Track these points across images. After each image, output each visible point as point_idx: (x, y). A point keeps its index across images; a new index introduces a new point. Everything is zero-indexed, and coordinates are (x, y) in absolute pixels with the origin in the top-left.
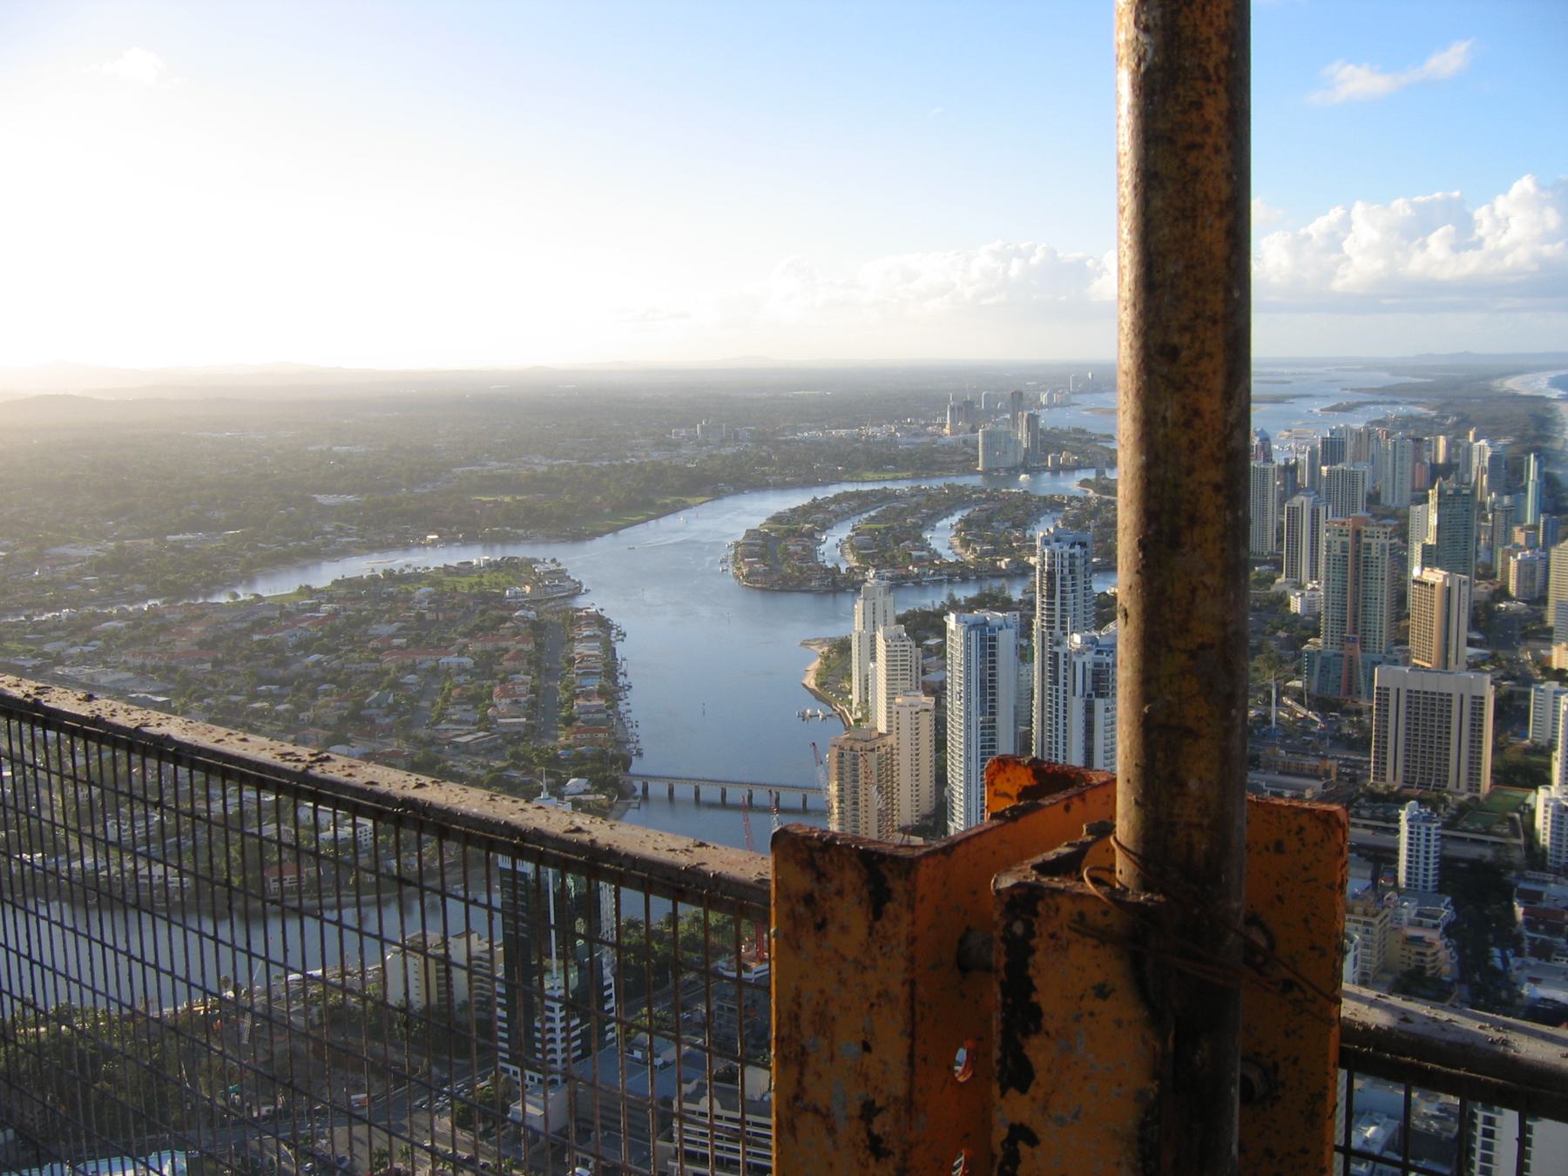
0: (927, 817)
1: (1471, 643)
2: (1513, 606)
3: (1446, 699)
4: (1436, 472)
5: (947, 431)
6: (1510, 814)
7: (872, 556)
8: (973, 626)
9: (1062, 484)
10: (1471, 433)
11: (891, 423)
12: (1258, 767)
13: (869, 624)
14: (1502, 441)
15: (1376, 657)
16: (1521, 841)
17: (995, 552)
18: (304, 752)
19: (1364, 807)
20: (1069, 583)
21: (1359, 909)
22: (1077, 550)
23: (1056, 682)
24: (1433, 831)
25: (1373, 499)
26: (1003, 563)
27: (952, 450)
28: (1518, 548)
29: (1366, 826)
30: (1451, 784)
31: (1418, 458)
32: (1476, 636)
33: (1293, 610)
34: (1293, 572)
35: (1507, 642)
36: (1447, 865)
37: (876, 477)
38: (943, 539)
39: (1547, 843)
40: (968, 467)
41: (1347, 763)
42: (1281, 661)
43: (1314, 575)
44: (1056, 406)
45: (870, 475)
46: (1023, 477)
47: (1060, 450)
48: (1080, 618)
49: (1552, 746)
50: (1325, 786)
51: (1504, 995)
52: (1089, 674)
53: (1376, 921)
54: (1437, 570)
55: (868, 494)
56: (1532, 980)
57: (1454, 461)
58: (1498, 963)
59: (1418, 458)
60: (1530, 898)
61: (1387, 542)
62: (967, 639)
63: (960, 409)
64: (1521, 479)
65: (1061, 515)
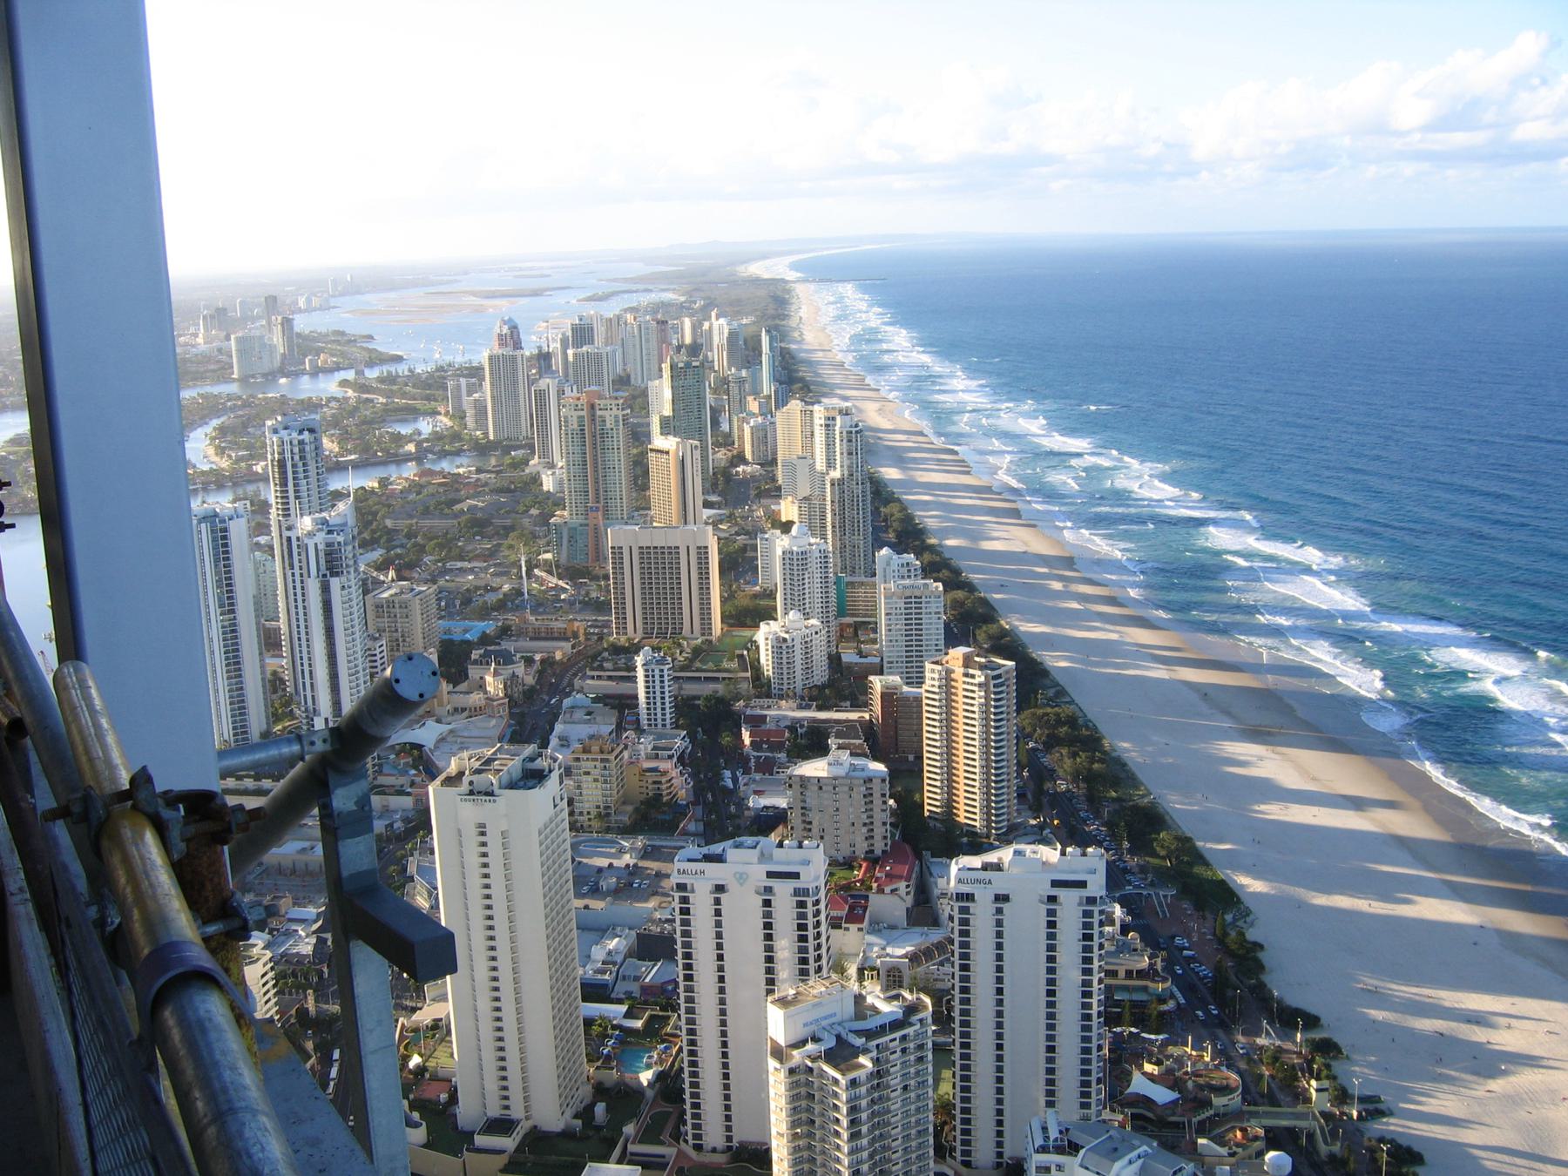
1: (707, 505)
2: (749, 469)
5: (200, 340)
17: (251, 457)
20: (301, 469)
21: (595, 748)
22: (306, 436)
27: (205, 359)
29: (610, 678)
31: (663, 340)
32: (714, 498)
33: (545, 488)
34: (545, 453)
35: (740, 501)
42: (534, 536)
44: (315, 310)
46: (283, 381)
47: (318, 352)
52: (322, 554)
53: (612, 757)
54: (671, 438)
56: (757, 793)
58: (730, 784)
59: (663, 340)
61: (620, 413)
63: (212, 317)
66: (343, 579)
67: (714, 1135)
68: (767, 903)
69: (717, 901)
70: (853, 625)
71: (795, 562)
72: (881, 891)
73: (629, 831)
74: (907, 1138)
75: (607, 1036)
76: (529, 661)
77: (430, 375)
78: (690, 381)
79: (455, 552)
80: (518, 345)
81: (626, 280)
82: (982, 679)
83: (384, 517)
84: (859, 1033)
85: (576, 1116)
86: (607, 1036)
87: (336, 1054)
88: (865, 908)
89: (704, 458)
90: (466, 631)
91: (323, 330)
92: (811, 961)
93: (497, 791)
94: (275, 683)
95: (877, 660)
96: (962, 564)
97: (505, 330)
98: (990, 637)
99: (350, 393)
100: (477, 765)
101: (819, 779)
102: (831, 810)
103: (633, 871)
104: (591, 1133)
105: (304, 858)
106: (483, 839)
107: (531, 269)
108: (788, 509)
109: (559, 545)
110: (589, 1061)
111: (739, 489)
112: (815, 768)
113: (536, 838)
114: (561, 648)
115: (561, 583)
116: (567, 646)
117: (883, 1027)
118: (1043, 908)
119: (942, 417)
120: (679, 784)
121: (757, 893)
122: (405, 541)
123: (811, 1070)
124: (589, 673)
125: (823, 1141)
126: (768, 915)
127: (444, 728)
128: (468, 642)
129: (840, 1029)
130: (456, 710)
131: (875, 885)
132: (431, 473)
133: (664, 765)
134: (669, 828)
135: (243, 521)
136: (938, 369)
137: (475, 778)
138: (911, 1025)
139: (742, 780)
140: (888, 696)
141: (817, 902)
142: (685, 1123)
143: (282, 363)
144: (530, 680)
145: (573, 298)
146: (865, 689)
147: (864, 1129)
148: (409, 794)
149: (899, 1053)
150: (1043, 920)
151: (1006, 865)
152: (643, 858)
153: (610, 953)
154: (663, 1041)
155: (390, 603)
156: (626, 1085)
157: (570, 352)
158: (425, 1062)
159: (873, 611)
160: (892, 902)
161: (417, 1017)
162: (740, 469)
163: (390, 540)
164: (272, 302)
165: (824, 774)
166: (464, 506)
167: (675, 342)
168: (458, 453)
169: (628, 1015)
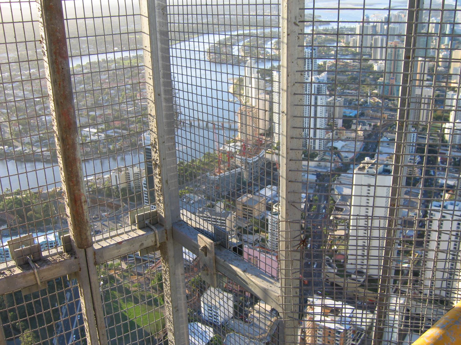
12: (364, 116)
18: (51, 102)
41: (390, 115)
52: (316, 88)
90: (350, 113)
128: (351, 117)
137: (369, 170)
139: (437, 173)
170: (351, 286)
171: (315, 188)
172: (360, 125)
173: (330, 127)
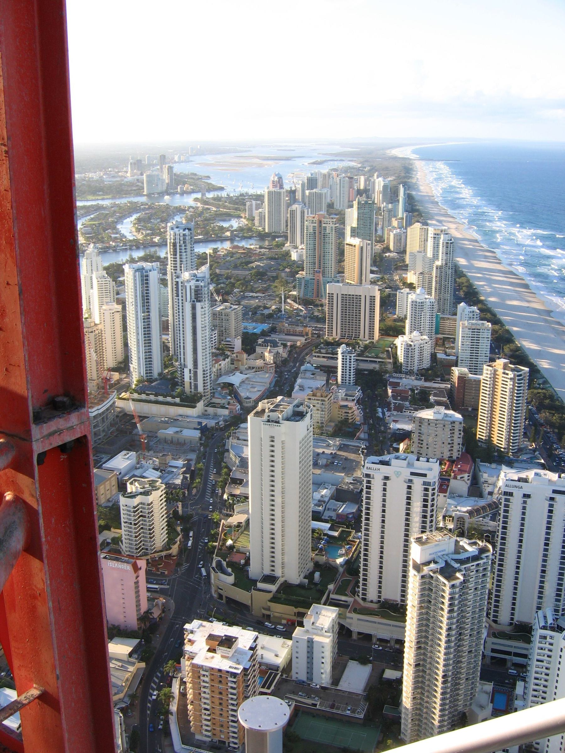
0: (121, 363)
1: (372, 272)
3: (358, 298)
4: (360, 192)
5: (129, 175)
6: (387, 349)
7: (92, 238)
8: (137, 270)
9: (185, 200)
10: (375, 175)
11: (101, 171)
12: (276, 332)
13: (90, 271)
14: (390, 179)
15: (329, 280)
16: (391, 361)
17: (153, 234)
19: (323, 348)
20: (183, 248)
21: (319, 394)
22: (187, 232)
23: (178, 296)
24: (352, 358)
25: (330, 206)
26: (156, 239)
27: (131, 184)
28: (394, 228)
29: (324, 357)
30: (361, 337)
31: (351, 187)
32: (375, 269)
34: (293, 241)
36: (359, 373)
37: (94, 198)
38: (127, 228)
39: (402, 361)
40: (139, 192)
42: (287, 283)
43: (302, 243)
45: (90, 197)
47: (184, 183)
48: (189, 264)
49: (406, 318)
50: (306, 340)
51: (382, 428)
53: (326, 399)
54: (357, 238)
55: (92, 206)
56: (394, 421)
57: (368, 188)
58: (380, 415)
59: (351, 187)
60: (395, 385)
61: (334, 226)
62: (135, 276)
63: (135, 164)
64: (397, 196)
65: (184, 215)
66: (202, 303)
67: (372, 594)
68: (409, 487)
69: (385, 484)
70: (443, 339)
71: (418, 306)
72: (455, 478)
73: (334, 435)
74: (474, 612)
75: (321, 539)
76: (285, 346)
77: (237, 197)
78: (367, 210)
79: (249, 288)
80: (281, 187)
81: (331, 154)
82: (512, 376)
83: (216, 268)
84: (457, 561)
85: (305, 578)
86: (321, 539)
87: (191, 534)
88: (448, 486)
89: (372, 248)
90: (255, 328)
91: (187, 173)
92: (428, 517)
93: (281, 421)
94: (165, 348)
95: (454, 358)
96: (497, 310)
97: (276, 179)
98: (511, 350)
99: (199, 205)
100: (271, 407)
101: (429, 420)
102: (433, 435)
103: (334, 456)
104: (312, 587)
105: (176, 436)
106: (272, 443)
107: (286, 146)
108: (411, 277)
109: (300, 288)
110: (312, 550)
111: (387, 265)
112: (427, 414)
113: (298, 445)
114: (300, 340)
115: (300, 307)
116: (303, 339)
117: (468, 558)
118: (547, 503)
119: (489, 234)
120: (357, 414)
121: (405, 482)
122: (225, 280)
123: (432, 577)
124: (314, 354)
125: (435, 611)
126: (409, 493)
127: (244, 377)
129: (447, 558)
130: (250, 368)
131: (453, 474)
132: (237, 247)
133: (351, 404)
134: (351, 435)
135: (156, 272)
136: (546, 252)
137: (271, 414)
138: (482, 559)
140: (461, 378)
141: (434, 489)
142: (358, 587)
143: (167, 188)
144: (285, 355)
145: (306, 162)
146: (450, 373)
147: (456, 608)
148: (227, 408)
149: (475, 572)
150: (547, 508)
151: (530, 480)
152: (339, 450)
153: (322, 496)
154: (348, 544)
155: (220, 313)
156: (330, 564)
157: (307, 192)
158: (234, 543)
159: (454, 332)
160: (461, 484)
161: (230, 520)
162: (387, 255)
163: (218, 280)
164: (163, 158)
165: (431, 417)
166: (254, 265)
167: (356, 188)
168: (250, 238)
169: (331, 529)
170: (258, 599)
171: (199, 450)
172: (268, 346)
173: (221, 351)
